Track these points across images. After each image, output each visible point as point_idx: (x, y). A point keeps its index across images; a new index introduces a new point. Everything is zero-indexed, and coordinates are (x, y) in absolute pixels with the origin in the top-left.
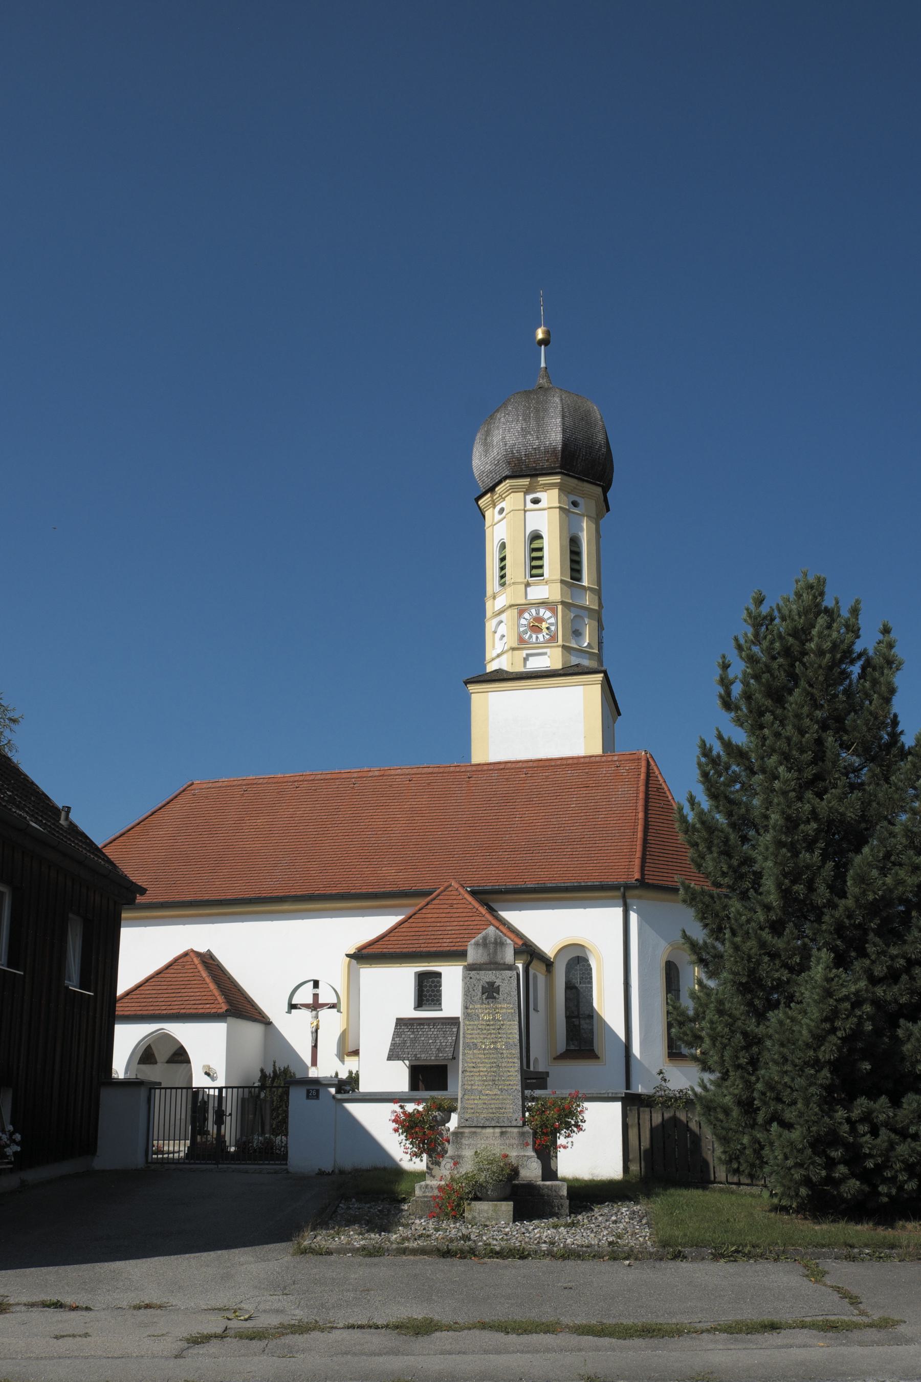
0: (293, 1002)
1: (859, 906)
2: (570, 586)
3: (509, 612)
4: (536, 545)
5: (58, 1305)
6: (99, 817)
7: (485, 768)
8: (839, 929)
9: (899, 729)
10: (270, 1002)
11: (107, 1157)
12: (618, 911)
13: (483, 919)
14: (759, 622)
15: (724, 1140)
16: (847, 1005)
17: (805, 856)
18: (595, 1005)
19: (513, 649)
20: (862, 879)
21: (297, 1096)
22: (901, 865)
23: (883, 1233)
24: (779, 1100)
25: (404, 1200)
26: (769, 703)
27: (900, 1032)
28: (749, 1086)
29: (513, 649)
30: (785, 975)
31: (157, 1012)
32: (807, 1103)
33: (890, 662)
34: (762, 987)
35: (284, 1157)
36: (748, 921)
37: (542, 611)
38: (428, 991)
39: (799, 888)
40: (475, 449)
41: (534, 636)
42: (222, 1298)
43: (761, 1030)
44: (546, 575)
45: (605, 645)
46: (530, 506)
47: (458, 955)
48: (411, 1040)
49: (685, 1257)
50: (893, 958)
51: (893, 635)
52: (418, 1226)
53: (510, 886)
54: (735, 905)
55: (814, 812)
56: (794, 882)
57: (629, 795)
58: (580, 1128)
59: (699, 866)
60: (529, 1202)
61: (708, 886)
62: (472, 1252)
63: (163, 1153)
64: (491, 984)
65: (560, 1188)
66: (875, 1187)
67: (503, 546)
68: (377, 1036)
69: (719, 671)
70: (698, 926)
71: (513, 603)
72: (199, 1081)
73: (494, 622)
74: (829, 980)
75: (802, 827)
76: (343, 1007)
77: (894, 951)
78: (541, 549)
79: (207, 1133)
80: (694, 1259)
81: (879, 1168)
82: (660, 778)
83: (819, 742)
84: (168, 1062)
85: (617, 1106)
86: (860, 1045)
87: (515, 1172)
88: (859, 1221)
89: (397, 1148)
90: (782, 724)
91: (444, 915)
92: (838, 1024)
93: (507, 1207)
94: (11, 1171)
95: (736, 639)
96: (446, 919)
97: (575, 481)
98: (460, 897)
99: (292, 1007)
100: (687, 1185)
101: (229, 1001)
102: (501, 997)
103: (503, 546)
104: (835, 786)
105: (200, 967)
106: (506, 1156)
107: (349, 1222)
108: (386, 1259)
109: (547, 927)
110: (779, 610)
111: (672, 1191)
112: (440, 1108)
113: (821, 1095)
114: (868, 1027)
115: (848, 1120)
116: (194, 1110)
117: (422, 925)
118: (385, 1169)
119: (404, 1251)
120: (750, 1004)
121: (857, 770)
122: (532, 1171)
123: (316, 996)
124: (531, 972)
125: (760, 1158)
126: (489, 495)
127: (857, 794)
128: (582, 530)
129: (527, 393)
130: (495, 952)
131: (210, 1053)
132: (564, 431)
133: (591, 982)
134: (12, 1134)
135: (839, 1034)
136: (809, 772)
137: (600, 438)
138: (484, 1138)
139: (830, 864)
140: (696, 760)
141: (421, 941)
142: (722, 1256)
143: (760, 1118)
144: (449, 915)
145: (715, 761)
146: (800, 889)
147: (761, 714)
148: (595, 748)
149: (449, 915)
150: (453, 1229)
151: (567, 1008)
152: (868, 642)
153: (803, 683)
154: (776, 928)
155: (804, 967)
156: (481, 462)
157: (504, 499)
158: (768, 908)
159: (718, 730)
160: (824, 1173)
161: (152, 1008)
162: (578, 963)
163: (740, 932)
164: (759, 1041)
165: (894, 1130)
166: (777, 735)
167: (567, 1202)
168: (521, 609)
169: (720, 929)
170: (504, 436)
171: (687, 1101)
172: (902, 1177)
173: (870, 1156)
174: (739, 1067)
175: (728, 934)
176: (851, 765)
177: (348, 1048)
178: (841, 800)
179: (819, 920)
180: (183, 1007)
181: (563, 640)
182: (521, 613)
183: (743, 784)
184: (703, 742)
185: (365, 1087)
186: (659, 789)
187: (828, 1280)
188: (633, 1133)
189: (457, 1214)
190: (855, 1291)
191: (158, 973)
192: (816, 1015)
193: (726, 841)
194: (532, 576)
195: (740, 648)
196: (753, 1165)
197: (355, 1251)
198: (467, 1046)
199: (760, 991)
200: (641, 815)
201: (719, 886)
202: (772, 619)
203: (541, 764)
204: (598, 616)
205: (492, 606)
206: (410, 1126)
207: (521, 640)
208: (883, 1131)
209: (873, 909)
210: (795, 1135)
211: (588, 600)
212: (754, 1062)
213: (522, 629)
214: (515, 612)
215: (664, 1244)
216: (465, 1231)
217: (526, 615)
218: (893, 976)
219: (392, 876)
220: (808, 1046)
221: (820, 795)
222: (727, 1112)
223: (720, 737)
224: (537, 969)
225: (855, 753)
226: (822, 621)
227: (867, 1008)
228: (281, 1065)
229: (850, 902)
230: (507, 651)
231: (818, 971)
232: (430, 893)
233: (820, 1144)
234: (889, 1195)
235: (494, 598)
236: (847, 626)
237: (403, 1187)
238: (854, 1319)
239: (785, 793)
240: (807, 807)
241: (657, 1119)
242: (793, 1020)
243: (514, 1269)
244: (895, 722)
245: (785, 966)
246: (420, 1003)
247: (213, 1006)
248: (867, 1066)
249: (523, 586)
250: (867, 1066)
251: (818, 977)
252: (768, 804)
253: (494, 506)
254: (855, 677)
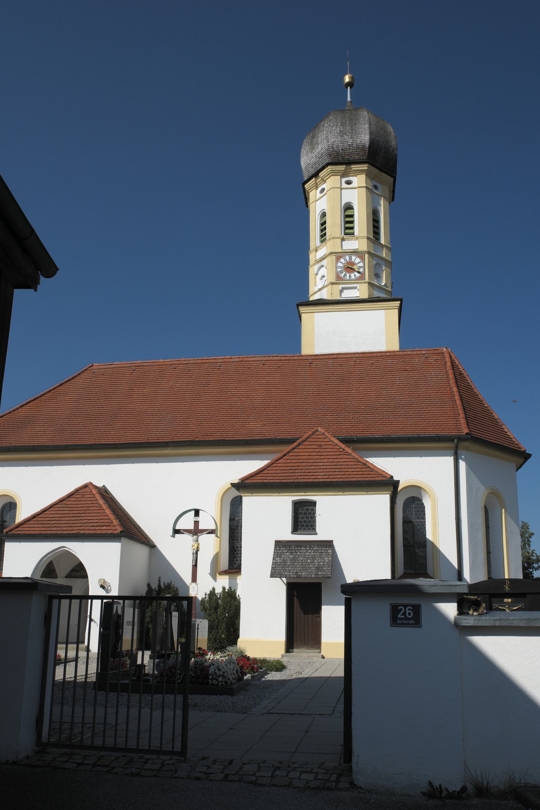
0: (177, 528)
2: (373, 242)
3: (329, 258)
4: (349, 213)
7: (322, 357)
12: (450, 460)
13: (350, 457)
18: (429, 536)
19: (332, 284)
29: (332, 284)
31: (59, 532)
37: (354, 258)
38: (303, 518)
40: (303, 150)
41: (348, 275)
44: (356, 234)
46: (344, 185)
48: (291, 560)
67: (324, 215)
71: (333, 251)
73: (316, 267)
78: (352, 216)
82: (460, 367)
91: (315, 454)
96: (317, 457)
97: (377, 171)
98: (327, 440)
99: (176, 532)
103: (324, 215)
105: (98, 497)
117: (296, 461)
123: (196, 523)
126: (314, 179)
128: (380, 205)
132: (371, 134)
133: (424, 517)
141: (297, 474)
144: (319, 454)
149: (319, 454)
156: (307, 159)
157: (325, 182)
161: (55, 529)
168: (339, 256)
170: (329, 136)
180: (82, 528)
181: (369, 279)
182: (338, 259)
194: (345, 234)
203: (365, 355)
205: (313, 257)
207: (338, 277)
213: (339, 270)
214: (334, 258)
217: (342, 260)
219: (257, 428)
228: (165, 581)
230: (327, 285)
235: (316, 251)
246: (296, 529)
247: (109, 528)
249: (340, 240)
253: (317, 188)
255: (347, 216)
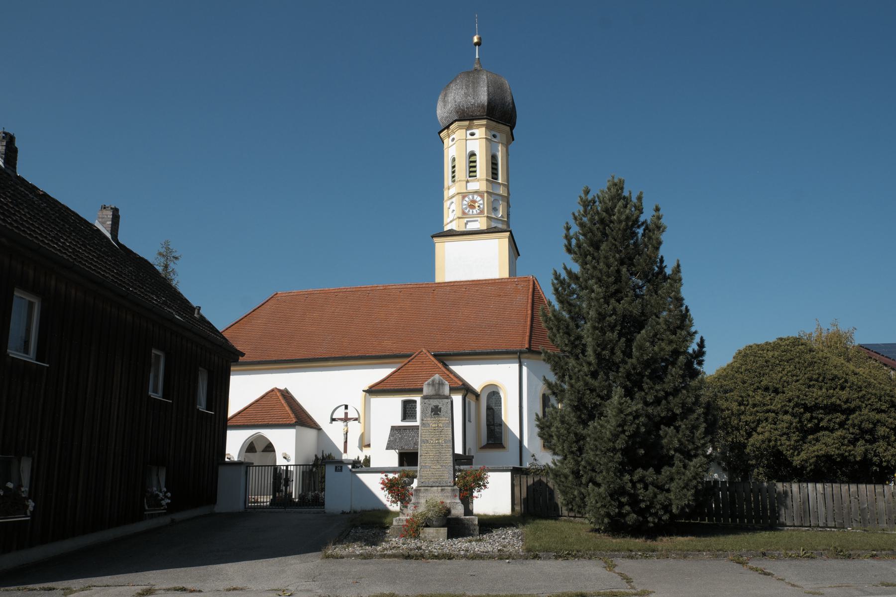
1: (639, 363)
5: (183, 589)
6: (220, 313)
8: (628, 376)
9: (664, 264)
10: (320, 417)
11: (223, 505)
12: (516, 366)
14: (586, 204)
15: (564, 493)
16: (631, 417)
17: (609, 334)
18: (503, 418)
19: (459, 218)
20: (641, 348)
21: (330, 470)
22: (662, 340)
23: (649, 542)
24: (593, 470)
25: (388, 528)
26: (591, 249)
27: (661, 432)
28: (578, 463)
29: (459, 218)
30: (598, 401)
32: (608, 471)
33: (659, 228)
34: (586, 408)
35: (323, 504)
36: (579, 371)
39: (606, 353)
42: (277, 584)
43: (585, 432)
45: (511, 216)
46: (469, 137)
47: (419, 391)
49: (540, 558)
50: (657, 391)
51: (661, 213)
52: (394, 542)
53: (456, 351)
54: (572, 362)
55: (614, 309)
56: (603, 349)
57: (523, 300)
58: (485, 486)
59: (553, 341)
60: (456, 528)
61: (557, 351)
62: (422, 556)
63: (257, 502)
64: (437, 407)
65: (474, 520)
66: (645, 518)
67: (454, 160)
68: (380, 436)
69: (565, 231)
70: (552, 374)
72: (280, 462)
74: (621, 404)
75: (608, 318)
76: (362, 420)
77: (658, 387)
79: (282, 491)
80: (545, 559)
81: (648, 508)
83: (618, 271)
84: (263, 451)
85: (509, 474)
86: (638, 440)
87: (449, 511)
88: (637, 537)
89: (384, 497)
90: (598, 263)
92: (626, 428)
93: (444, 531)
94: (165, 514)
95: (574, 214)
99: (333, 420)
100: (547, 517)
101: (297, 417)
102: (442, 414)
103: (454, 160)
104: (627, 296)
105: (281, 398)
106: (442, 503)
107: (355, 540)
108: (374, 560)
109: (476, 375)
110: (598, 197)
111: (538, 521)
112: (408, 476)
113: (616, 468)
114: (643, 429)
115: (631, 481)
116: (275, 478)
118: (379, 510)
119: (384, 556)
120: (579, 417)
121: (640, 288)
122: (458, 510)
123: (346, 414)
124: (467, 400)
125: (584, 502)
127: (639, 301)
129: (468, 73)
130: (439, 388)
131: (286, 446)
132: (488, 95)
133: (500, 406)
134: (166, 493)
135: (627, 434)
136: (613, 289)
137: (509, 99)
138: (432, 492)
139: (623, 340)
140: (550, 282)
142: (560, 557)
143: (584, 480)
145: (562, 282)
146: (606, 353)
147: (586, 256)
148: (506, 275)
150: (413, 543)
151: (488, 420)
152: (647, 216)
153: (610, 238)
154: (594, 375)
155: (609, 397)
156: (442, 111)
158: (589, 364)
159: (678, 261)
160: (617, 510)
162: (494, 395)
163: (574, 377)
164: (583, 438)
165: (657, 487)
166: (595, 268)
167: (478, 528)
168: (464, 196)
169: (564, 376)
170: (455, 97)
171: (546, 470)
172: (661, 512)
173: (643, 501)
174: (572, 452)
175: (567, 378)
176: (637, 284)
177: (364, 444)
178: (630, 303)
179: (617, 372)
182: (464, 197)
183: (578, 295)
184: (555, 272)
185: (373, 465)
186: (540, 297)
187: (617, 570)
188: (517, 489)
189: (416, 535)
190: (630, 575)
191: (257, 401)
192: (614, 423)
193: (567, 327)
195: (575, 218)
196: (579, 507)
197: (357, 556)
198: (423, 441)
199: (586, 411)
200: (529, 312)
201: (564, 351)
202: (594, 202)
204: (507, 200)
205: (447, 193)
206: (390, 486)
207: (464, 213)
208: (650, 487)
209: (647, 364)
210: (602, 490)
211: (501, 191)
212: (581, 450)
214: (460, 197)
215: (529, 550)
216: (419, 544)
217: (467, 199)
218: (657, 401)
219: (389, 346)
220: (610, 440)
221: (619, 301)
222: (566, 477)
223: (565, 268)
224: (471, 398)
225: (639, 278)
226: (621, 203)
227: (642, 419)
228: (327, 453)
229: (634, 361)
231: (615, 399)
232: (411, 356)
233: (616, 494)
234: (654, 523)
236: (635, 206)
237: (387, 520)
238: (627, 591)
239: (598, 300)
240: (611, 307)
241: (530, 482)
242: (602, 426)
243: (445, 566)
244: (662, 261)
245: (599, 396)
248: (642, 451)
250: (642, 451)
251: (615, 403)
252: (590, 306)
254: (640, 235)
255: (471, 162)
